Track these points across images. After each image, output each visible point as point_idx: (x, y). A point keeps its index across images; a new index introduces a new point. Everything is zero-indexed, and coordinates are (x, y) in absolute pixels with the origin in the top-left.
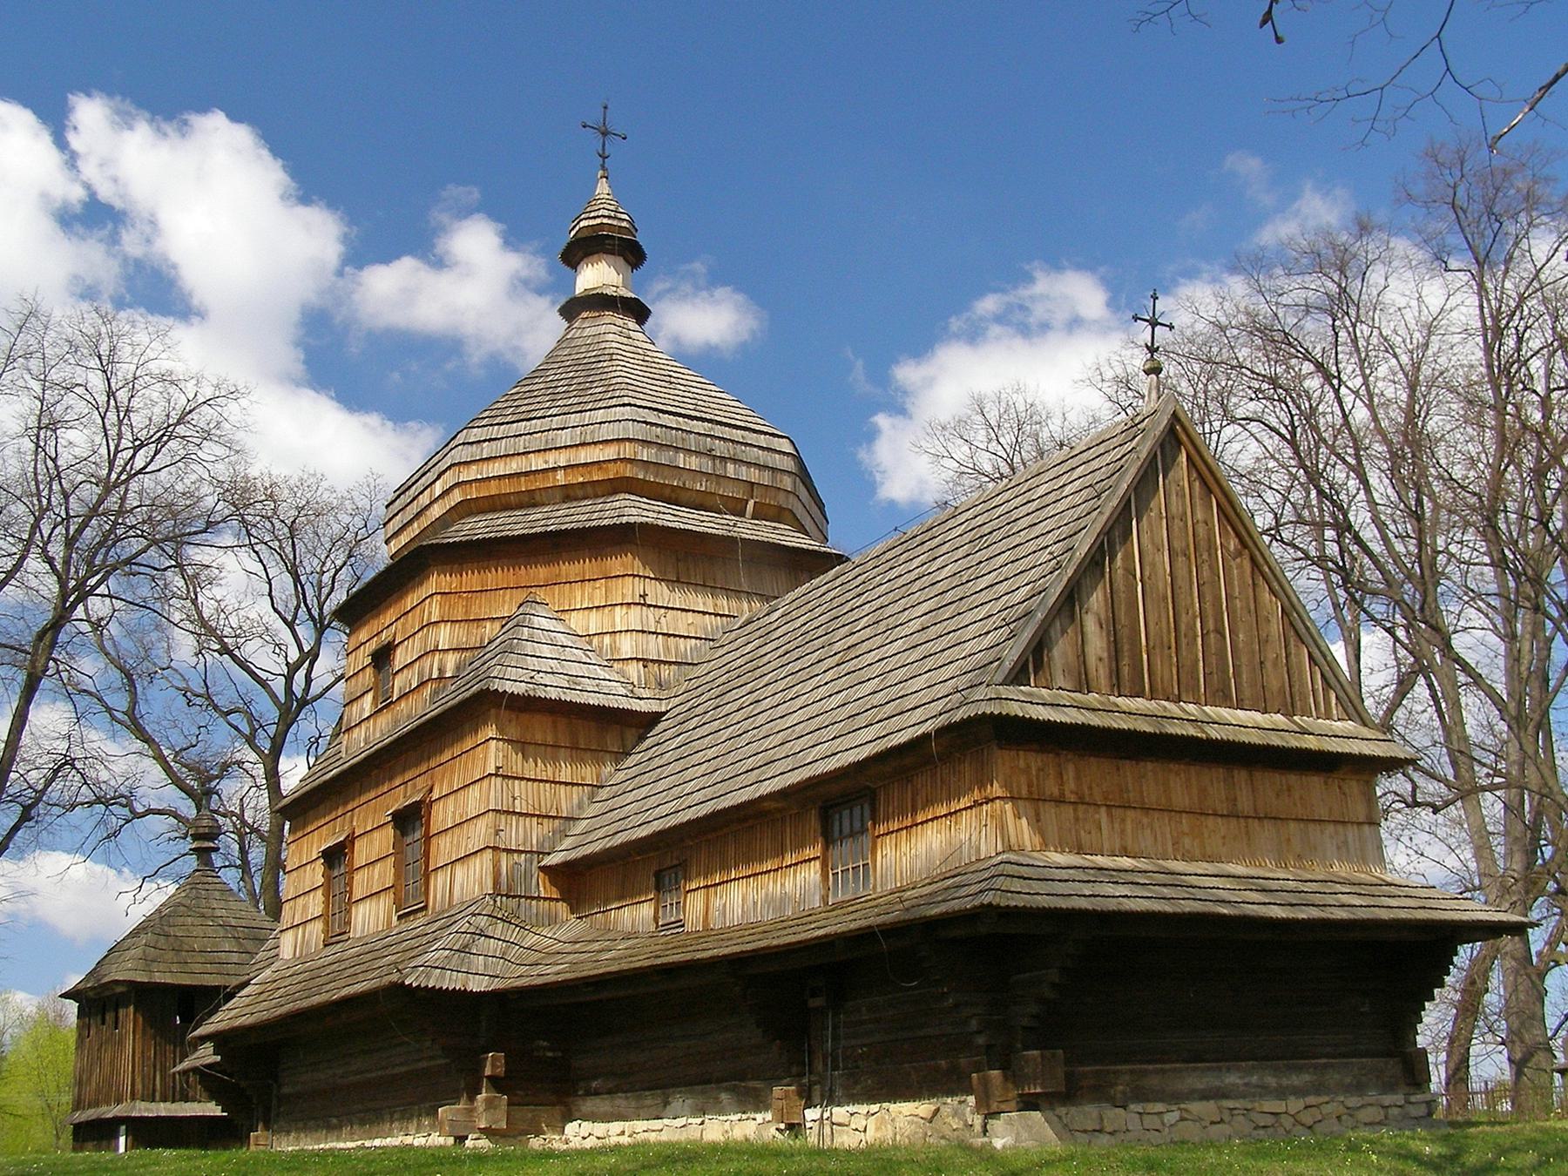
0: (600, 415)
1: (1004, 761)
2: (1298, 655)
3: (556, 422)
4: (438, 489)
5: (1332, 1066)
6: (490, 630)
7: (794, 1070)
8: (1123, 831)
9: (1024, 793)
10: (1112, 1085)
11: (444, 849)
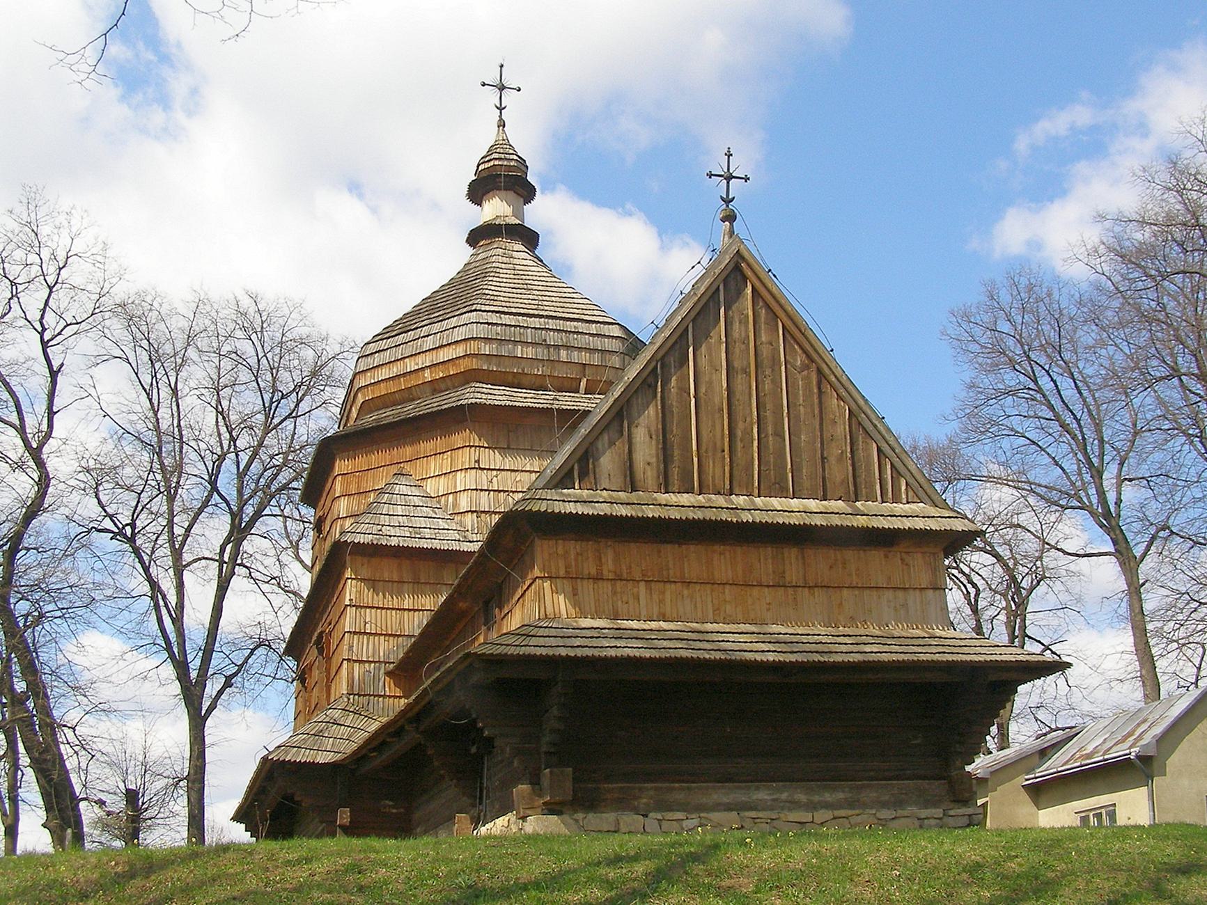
0: (453, 322)
1: (544, 551)
2: (867, 449)
5: (869, 786)
8: (661, 601)
9: (562, 573)
10: (636, 798)
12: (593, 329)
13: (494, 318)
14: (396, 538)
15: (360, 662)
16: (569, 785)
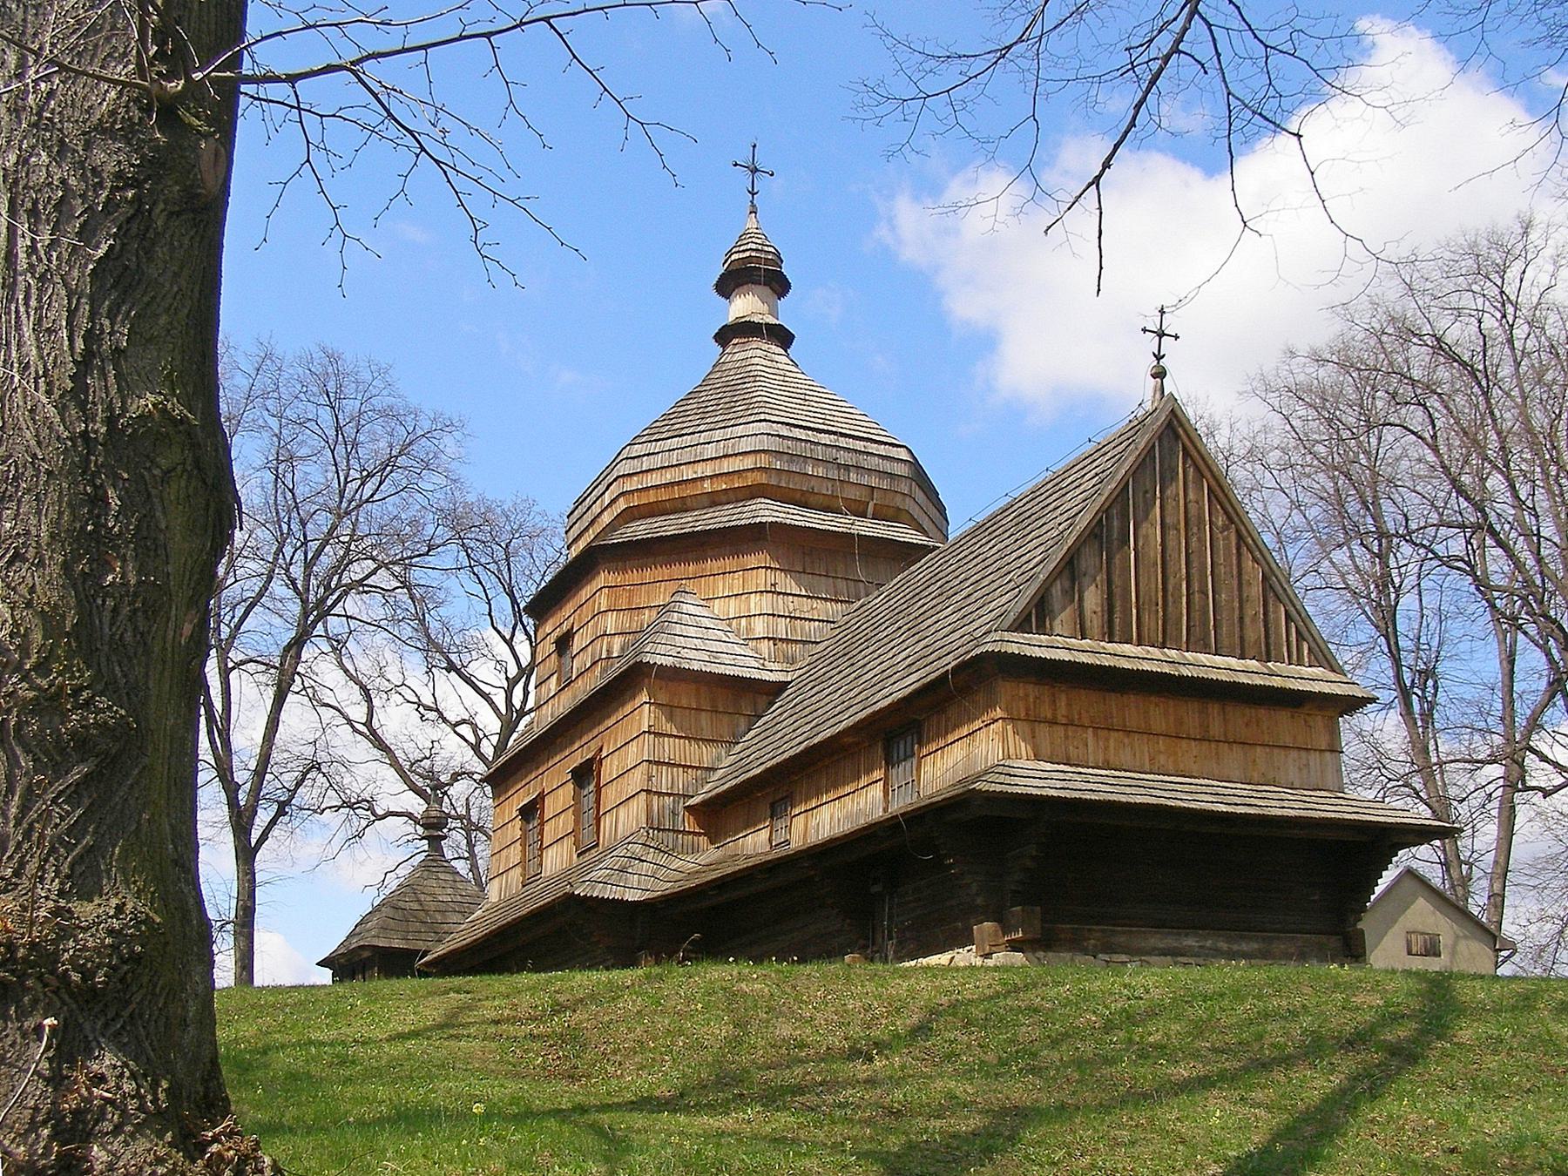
0: (739, 430)
1: (1006, 689)
2: (1276, 612)
3: (704, 437)
4: (607, 498)
6: (647, 616)
7: (862, 942)
8: (1106, 748)
9: (1022, 716)
11: (610, 796)
12: (882, 450)
13: (784, 431)
14: (696, 662)
15: (659, 794)
16: (1037, 923)
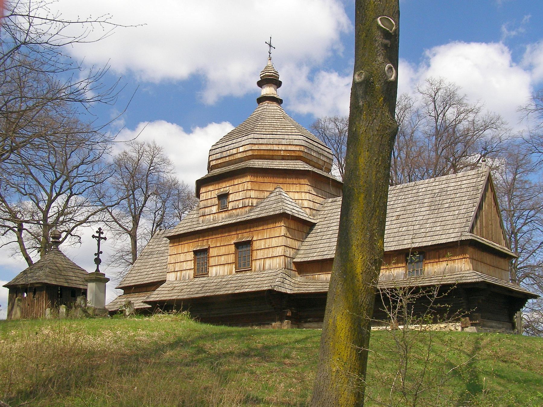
1: (470, 249)
